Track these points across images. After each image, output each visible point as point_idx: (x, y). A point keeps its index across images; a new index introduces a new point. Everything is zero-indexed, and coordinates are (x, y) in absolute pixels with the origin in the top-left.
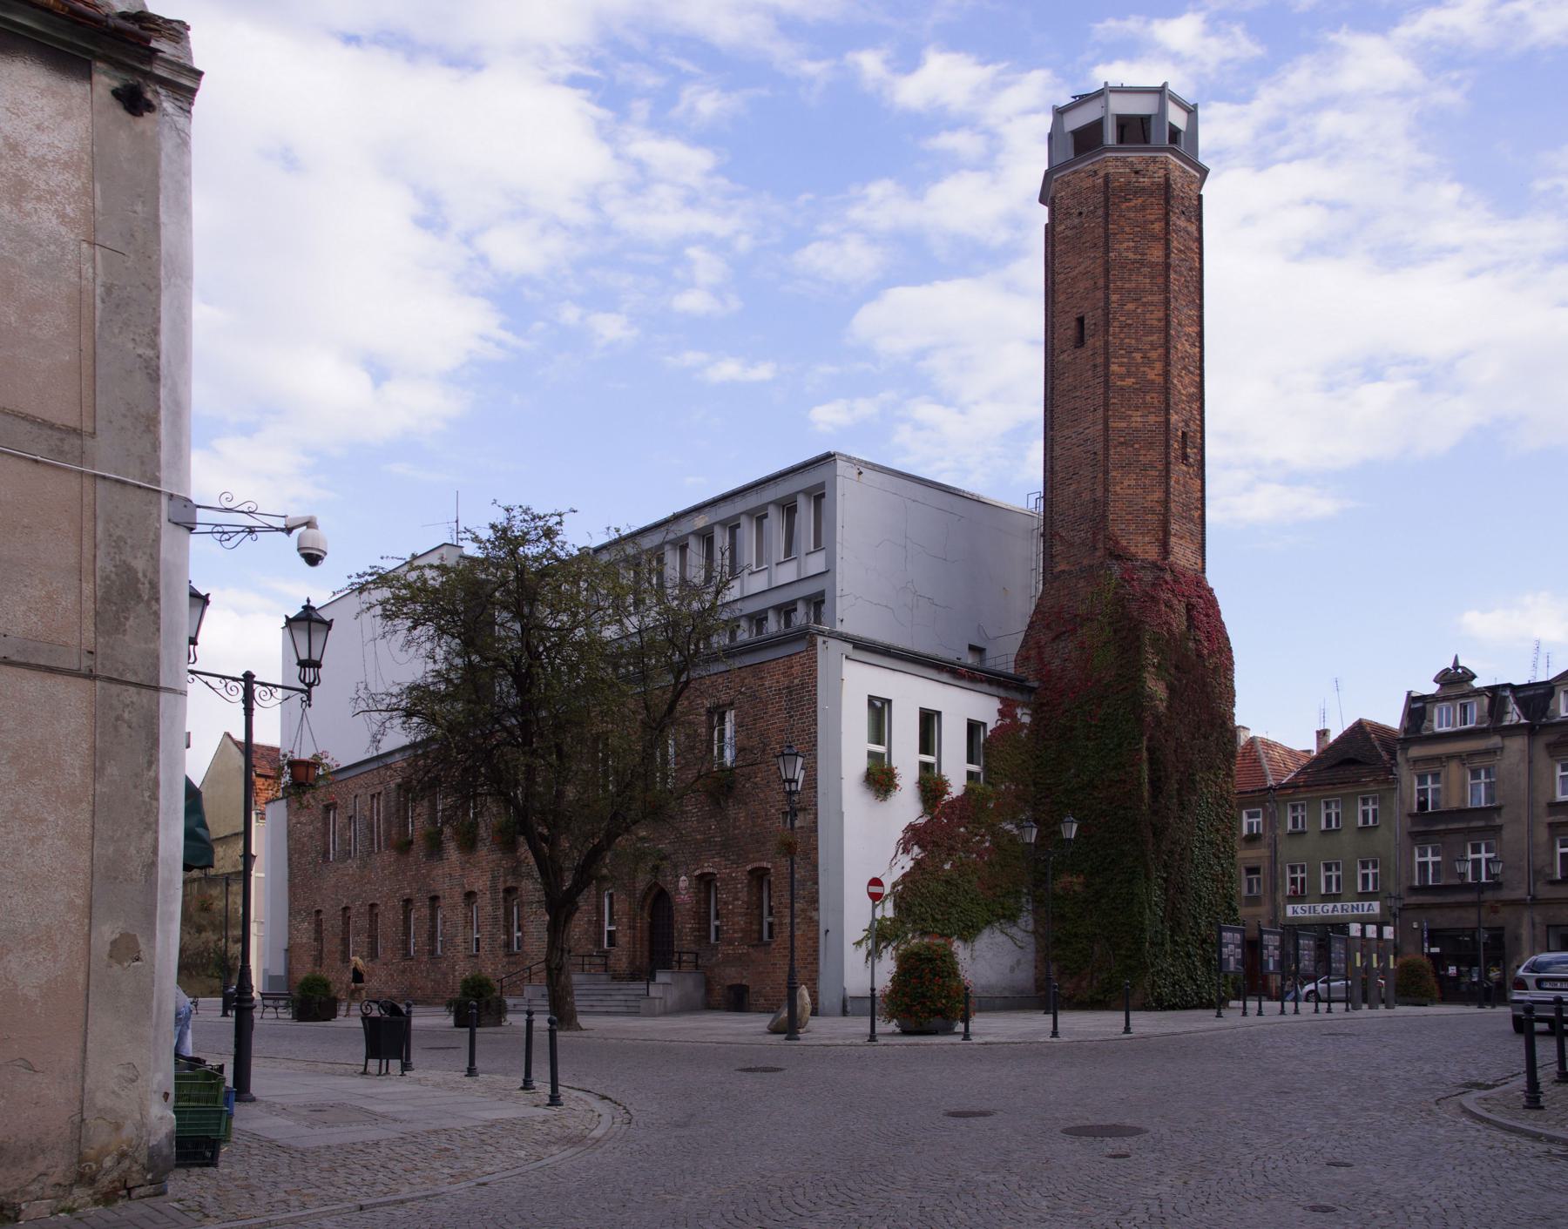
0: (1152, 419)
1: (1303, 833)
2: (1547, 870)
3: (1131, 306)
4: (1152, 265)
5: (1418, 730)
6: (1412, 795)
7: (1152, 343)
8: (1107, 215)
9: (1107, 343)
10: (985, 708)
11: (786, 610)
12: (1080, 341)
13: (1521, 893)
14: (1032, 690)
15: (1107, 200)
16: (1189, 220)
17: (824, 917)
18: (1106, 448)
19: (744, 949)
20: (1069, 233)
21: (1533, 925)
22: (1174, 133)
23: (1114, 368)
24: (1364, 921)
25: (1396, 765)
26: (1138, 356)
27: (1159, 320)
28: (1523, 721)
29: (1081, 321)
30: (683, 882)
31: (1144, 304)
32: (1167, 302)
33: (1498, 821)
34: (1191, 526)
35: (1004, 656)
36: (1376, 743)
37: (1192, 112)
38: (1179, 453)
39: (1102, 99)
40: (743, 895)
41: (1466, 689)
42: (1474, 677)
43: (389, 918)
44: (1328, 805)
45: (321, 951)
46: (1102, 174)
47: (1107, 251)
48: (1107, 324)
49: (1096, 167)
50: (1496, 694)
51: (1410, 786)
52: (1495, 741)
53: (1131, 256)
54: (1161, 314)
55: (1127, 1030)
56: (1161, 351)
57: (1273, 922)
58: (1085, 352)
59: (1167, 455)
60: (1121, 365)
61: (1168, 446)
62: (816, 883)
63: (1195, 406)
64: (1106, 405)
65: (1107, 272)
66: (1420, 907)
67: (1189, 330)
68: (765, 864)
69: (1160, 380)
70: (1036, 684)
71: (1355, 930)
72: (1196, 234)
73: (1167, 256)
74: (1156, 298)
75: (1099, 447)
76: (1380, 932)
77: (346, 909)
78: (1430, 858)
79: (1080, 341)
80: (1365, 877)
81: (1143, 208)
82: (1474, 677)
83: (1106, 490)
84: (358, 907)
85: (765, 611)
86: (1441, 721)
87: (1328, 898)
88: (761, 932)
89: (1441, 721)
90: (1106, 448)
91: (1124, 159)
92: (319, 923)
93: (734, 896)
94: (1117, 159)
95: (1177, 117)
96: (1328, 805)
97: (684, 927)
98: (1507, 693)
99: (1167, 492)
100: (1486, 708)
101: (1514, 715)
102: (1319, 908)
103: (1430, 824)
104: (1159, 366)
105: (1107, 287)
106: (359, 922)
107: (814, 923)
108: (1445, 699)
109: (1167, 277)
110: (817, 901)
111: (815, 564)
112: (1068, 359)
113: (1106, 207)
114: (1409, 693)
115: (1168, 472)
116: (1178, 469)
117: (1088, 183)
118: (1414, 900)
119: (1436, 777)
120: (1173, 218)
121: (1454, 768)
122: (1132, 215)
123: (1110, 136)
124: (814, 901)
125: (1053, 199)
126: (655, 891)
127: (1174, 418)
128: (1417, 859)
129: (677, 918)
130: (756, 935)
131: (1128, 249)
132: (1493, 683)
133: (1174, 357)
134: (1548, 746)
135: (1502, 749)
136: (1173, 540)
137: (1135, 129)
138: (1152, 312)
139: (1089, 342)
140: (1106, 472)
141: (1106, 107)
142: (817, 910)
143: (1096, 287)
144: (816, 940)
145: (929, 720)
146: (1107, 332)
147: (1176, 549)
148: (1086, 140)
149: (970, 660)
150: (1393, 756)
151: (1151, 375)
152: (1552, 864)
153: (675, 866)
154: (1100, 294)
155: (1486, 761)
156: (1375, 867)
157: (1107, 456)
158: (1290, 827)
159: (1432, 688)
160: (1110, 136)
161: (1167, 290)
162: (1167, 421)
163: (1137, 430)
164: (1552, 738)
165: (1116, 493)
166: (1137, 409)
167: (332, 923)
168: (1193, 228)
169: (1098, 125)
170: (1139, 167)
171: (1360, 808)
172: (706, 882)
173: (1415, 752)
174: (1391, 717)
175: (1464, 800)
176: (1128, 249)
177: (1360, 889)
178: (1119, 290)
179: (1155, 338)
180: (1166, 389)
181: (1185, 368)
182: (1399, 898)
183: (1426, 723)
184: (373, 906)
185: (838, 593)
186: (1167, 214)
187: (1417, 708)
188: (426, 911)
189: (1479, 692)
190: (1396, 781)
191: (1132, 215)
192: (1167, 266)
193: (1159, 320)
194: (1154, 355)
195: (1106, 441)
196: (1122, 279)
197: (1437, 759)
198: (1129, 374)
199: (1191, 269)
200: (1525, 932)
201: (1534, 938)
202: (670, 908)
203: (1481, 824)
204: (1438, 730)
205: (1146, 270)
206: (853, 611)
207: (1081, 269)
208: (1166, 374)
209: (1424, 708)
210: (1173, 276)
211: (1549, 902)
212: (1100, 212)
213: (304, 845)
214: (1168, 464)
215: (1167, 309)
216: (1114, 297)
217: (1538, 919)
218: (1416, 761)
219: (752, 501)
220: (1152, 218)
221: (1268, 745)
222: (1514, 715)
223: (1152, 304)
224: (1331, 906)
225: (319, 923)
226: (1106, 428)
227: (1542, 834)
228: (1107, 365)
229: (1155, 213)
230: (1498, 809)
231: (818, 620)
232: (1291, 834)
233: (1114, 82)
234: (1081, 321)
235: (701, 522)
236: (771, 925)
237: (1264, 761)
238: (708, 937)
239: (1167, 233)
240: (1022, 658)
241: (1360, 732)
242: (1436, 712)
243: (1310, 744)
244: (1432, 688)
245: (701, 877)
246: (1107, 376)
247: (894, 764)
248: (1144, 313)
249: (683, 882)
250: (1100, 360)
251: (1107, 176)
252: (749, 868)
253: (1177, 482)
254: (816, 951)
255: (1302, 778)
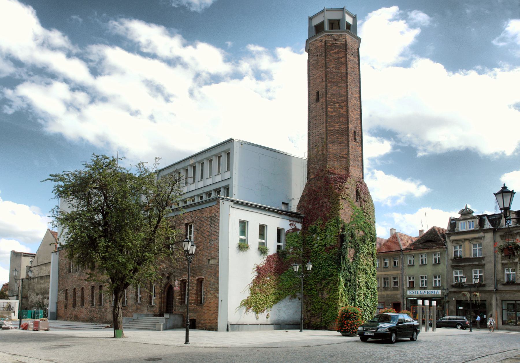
0: (343, 126)
1: (413, 265)
2: (502, 280)
3: (334, 88)
4: (341, 73)
5: (454, 231)
6: (452, 253)
7: (342, 100)
8: (326, 55)
9: (326, 100)
10: (285, 224)
11: (209, 194)
12: (318, 100)
13: (492, 288)
14: (302, 218)
15: (326, 50)
16: (354, 57)
17: (221, 296)
18: (327, 137)
19: (195, 306)
20: (314, 62)
21: (497, 300)
22: (349, 26)
23: (329, 109)
24: (424, 299)
25: (446, 242)
26: (337, 105)
27: (344, 92)
28: (491, 227)
29: (318, 93)
30: (177, 283)
31: (339, 87)
32: (347, 86)
33: (483, 262)
34: (358, 163)
35: (294, 208)
36: (439, 235)
37: (354, 18)
38: (353, 138)
39: (323, 13)
40: (195, 287)
41: (470, 216)
42: (473, 212)
43: (87, 292)
44: (422, 256)
45: (67, 304)
46: (324, 41)
47: (326, 69)
48: (326, 94)
49: (322, 39)
50: (481, 218)
51: (451, 249)
52: (481, 234)
53: (334, 70)
54: (345, 90)
55: (187, 341)
56: (345, 103)
57: (403, 296)
58: (319, 104)
59: (348, 139)
60: (331, 108)
61: (348, 136)
62: (218, 284)
63: (359, 122)
64: (326, 122)
65: (326, 75)
66: (455, 292)
67: (355, 96)
68: (202, 277)
69: (345, 113)
70: (303, 216)
71: (420, 302)
72: (357, 62)
73: (347, 70)
74: (343, 85)
75: (324, 136)
76: (430, 303)
77: (75, 289)
78: (459, 275)
79: (318, 100)
80: (435, 281)
81: (338, 53)
82: (473, 212)
83: (327, 151)
84: (78, 289)
85: (211, 191)
86: (462, 227)
87: (423, 288)
88: (201, 300)
89: (462, 227)
90: (327, 137)
91: (331, 35)
92: (66, 294)
93: (193, 288)
94: (329, 35)
95: (349, 20)
96: (422, 256)
97: (177, 297)
98: (486, 218)
99: (348, 152)
100: (478, 223)
101: (488, 225)
102: (419, 292)
103: (458, 262)
104: (344, 108)
105: (326, 81)
106: (79, 294)
107: (217, 298)
108: (463, 220)
109: (347, 77)
110: (218, 290)
111: (227, 175)
112: (314, 106)
113: (325, 53)
114: (450, 217)
115: (348, 144)
116: (352, 144)
117: (320, 44)
118: (453, 290)
119: (460, 246)
120: (348, 56)
121: (467, 243)
122: (334, 55)
123: (326, 27)
124: (217, 290)
125: (309, 50)
126: (169, 285)
127: (350, 126)
128: (454, 275)
129: (175, 295)
130: (199, 302)
131: (333, 68)
132: (481, 214)
133: (350, 105)
134: (501, 236)
135: (484, 237)
136: (351, 168)
137: (335, 24)
138: (342, 89)
139: (321, 100)
140: (327, 145)
141: (324, 16)
142: (218, 293)
143: (323, 82)
144: (218, 304)
145: (262, 229)
146: (326, 97)
147: (352, 171)
148: (319, 28)
149: (283, 208)
150: (445, 238)
151: (342, 111)
152: (503, 278)
153: (174, 277)
154: (324, 84)
155: (479, 241)
156: (439, 278)
157: (327, 140)
158: (408, 263)
159: (458, 216)
160: (326, 27)
161: (347, 82)
162: (348, 127)
163: (337, 130)
164: (502, 233)
165: (330, 152)
166: (337, 123)
167: (70, 294)
168: (356, 60)
169: (322, 23)
170: (336, 38)
171: (434, 257)
172: (183, 283)
173: (453, 238)
174: (444, 225)
175: (470, 255)
176: (333, 68)
177: (434, 286)
178: (330, 82)
179: (343, 98)
180: (347, 117)
181: (354, 109)
182: (448, 289)
183: (456, 228)
184: (83, 288)
185: (234, 185)
186: (346, 55)
187: (453, 223)
188: (98, 290)
189: (475, 217)
190: (446, 248)
191: (334, 55)
192: (347, 73)
193: (344, 92)
194: (343, 104)
195: (327, 134)
196: (331, 78)
197: (460, 240)
198: (334, 111)
199: (356, 74)
200: (494, 302)
201: (497, 304)
202: (173, 292)
203: (477, 263)
204: (461, 230)
205: (339, 75)
206: (236, 194)
207: (318, 75)
208: (347, 111)
209: (455, 223)
210: (349, 77)
211: (502, 292)
212: (324, 54)
213: (63, 267)
214: (348, 142)
215: (347, 88)
216: (329, 84)
217: (498, 298)
218: (453, 241)
219: (208, 155)
220: (341, 56)
221: (401, 235)
222: (488, 225)
223: (342, 86)
224: (423, 291)
225: (66, 294)
226: (327, 130)
227: (499, 267)
228: (326, 108)
229: (342, 55)
230: (483, 258)
231: (228, 195)
232: (409, 266)
233: (327, 7)
234: (318, 93)
235: (192, 161)
236: (204, 298)
237: (400, 240)
238: (184, 302)
239: (346, 62)
240: (299, 208)
241: (433, 231)
242: (460, 224)
243: (418, 235)
244: (458, 216)
245: (182, 281)
246: (326, 112)
247: (249, 244)
248: (339, 90)
249: (177, 283)
250: (324, 106)
251: (326, 41)
252: (197, 278)
253: (352, 148)
254: (218, 308)
255: (413, 246)
